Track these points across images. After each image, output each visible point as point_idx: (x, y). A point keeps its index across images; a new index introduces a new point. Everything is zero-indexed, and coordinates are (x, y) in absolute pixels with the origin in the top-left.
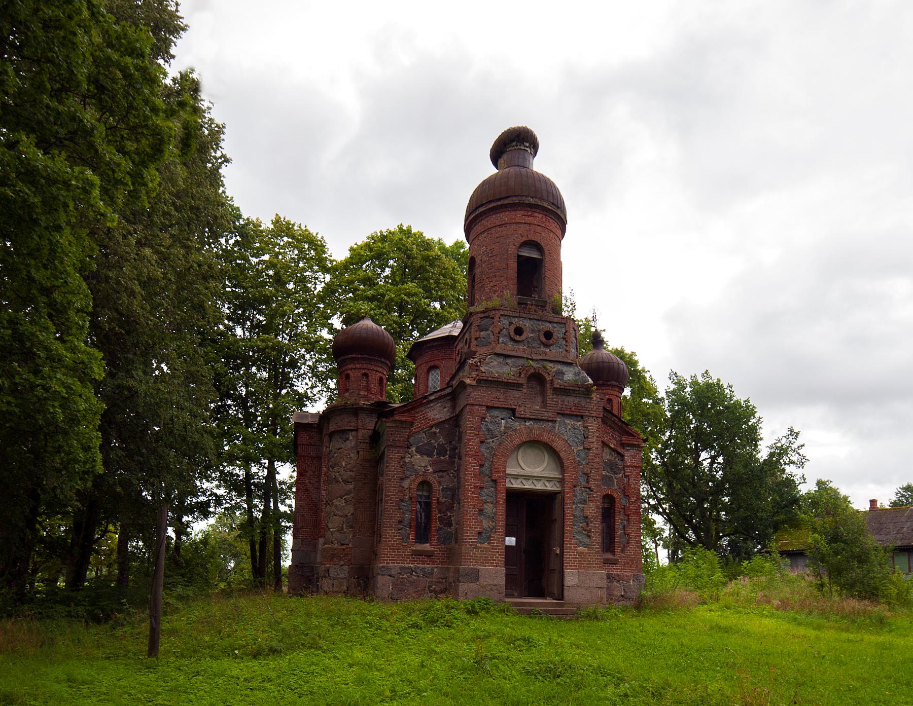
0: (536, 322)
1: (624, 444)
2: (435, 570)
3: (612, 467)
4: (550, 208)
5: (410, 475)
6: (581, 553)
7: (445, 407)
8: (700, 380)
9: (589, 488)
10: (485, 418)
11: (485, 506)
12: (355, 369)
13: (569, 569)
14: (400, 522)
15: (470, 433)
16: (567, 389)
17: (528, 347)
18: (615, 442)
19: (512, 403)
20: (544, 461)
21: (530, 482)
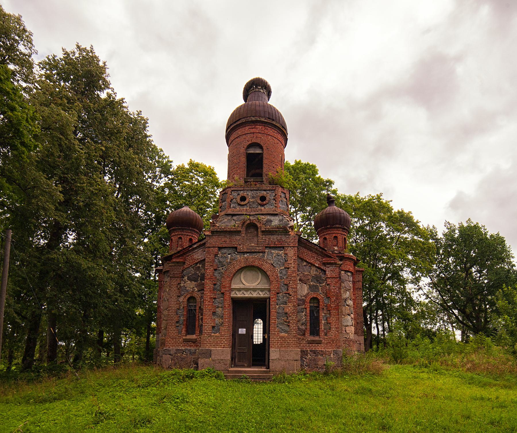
0: (255, 192)
1: (325, 263)
2: (197, 351)
3: (317, 279)
4: (266, 121)
5: (184, 294)
6: (282, 337)
7: (205, 251)
8: (465, 225)
9: (289, 294)
10: (217, 255)
11: (217, 310)
12: (175, 235)
13: (274, 348)
14: (177, 322)
15: (208, 265)
16: (271, 231)
17: (250, 208)
18: (319, 263)
19: (234, 244)
20: (258, 279)
21: (249, 292)
